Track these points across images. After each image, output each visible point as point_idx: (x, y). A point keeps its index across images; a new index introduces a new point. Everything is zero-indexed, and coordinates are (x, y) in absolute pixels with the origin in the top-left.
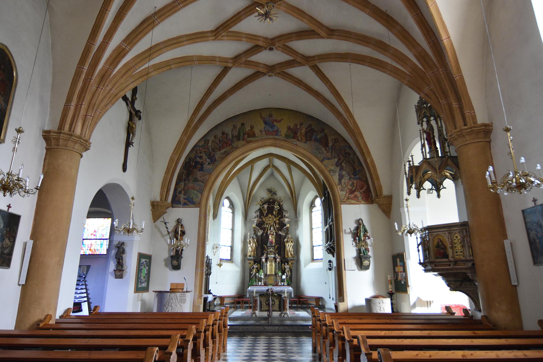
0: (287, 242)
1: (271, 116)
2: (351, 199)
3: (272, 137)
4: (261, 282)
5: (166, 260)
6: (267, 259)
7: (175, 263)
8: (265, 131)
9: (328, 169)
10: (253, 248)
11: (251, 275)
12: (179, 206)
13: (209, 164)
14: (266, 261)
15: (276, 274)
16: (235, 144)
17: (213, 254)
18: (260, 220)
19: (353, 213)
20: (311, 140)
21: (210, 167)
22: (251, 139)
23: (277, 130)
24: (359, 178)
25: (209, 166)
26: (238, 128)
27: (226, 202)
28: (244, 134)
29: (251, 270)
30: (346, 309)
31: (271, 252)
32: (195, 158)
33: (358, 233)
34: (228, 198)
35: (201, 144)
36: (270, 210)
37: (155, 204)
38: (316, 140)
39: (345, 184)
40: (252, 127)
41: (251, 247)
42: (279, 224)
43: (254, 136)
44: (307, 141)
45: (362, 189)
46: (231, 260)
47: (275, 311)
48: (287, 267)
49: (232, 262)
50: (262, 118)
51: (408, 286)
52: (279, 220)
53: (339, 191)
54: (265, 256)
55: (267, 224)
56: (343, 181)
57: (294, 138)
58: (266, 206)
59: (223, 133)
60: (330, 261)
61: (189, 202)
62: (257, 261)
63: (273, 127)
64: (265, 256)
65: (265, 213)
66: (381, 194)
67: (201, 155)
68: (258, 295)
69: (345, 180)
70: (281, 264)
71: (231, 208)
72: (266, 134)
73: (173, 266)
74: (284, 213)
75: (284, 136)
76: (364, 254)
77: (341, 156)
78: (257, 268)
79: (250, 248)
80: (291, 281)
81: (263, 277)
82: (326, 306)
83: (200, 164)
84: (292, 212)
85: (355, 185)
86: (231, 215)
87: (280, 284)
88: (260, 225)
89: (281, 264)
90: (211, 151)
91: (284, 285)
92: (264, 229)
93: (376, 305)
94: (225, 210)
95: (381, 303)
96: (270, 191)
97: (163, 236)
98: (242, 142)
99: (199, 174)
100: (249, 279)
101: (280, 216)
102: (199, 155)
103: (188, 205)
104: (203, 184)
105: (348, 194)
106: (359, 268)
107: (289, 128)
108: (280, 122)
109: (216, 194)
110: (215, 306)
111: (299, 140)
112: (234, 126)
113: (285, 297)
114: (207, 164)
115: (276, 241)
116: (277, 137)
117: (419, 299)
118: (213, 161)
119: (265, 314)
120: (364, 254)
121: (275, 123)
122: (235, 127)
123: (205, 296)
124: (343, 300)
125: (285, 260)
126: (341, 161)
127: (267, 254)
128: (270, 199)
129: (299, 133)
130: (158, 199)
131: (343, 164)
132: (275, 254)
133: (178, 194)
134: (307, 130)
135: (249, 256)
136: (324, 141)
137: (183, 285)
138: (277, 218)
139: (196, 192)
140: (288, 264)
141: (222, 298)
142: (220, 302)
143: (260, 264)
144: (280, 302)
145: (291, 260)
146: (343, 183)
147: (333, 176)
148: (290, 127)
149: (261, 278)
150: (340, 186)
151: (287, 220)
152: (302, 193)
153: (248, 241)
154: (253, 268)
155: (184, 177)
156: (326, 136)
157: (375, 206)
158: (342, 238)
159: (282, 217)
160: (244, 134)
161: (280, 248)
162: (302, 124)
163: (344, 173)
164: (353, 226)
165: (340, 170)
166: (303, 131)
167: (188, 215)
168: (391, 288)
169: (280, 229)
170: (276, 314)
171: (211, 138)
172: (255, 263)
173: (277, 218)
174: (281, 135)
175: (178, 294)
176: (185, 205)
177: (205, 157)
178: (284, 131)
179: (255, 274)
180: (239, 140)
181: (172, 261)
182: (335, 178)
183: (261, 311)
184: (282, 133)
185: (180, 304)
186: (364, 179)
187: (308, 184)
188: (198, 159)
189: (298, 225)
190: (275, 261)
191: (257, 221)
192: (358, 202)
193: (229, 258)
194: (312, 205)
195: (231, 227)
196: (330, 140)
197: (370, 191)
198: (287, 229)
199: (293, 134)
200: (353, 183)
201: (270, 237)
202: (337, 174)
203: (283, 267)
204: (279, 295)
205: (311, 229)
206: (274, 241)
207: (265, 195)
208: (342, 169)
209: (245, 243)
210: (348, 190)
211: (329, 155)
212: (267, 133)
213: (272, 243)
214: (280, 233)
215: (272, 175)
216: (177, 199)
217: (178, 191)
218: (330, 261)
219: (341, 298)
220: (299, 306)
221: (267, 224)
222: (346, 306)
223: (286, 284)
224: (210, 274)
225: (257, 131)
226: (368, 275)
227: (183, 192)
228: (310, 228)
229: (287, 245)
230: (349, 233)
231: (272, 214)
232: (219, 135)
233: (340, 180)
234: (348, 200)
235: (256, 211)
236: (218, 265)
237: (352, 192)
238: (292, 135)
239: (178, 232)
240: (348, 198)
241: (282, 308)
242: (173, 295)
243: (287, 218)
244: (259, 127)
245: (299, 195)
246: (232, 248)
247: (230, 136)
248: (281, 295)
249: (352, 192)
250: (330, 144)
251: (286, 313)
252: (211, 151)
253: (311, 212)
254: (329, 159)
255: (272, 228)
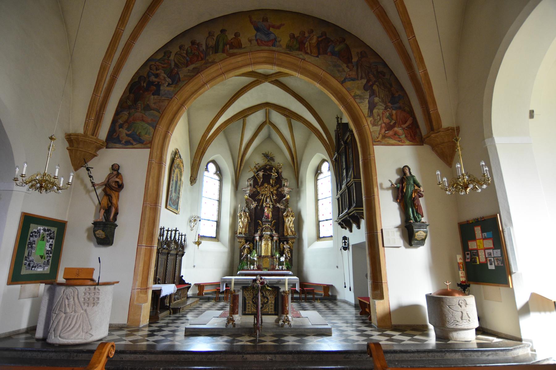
0: (287, 216)
1: (265, 20)
2: (389, 137)
3: (267, 48)
4: (254, 265)
5: (88, 230)
6: (261, 237)
7: (101, 233)
8: (257, 40)
9: (353, 94)
10: (245, 224)
11: (241, 256)
12: (118, 145)
13: (169, 85)
14: (261, 239)
15: (272, 256)
16: (210, 58)
17: (189, 228)
18: (254, 190)
19: (390, 160)
20: (327, 54)
21: (171, 89)
22: (235, 51)
23: (275, 39)
24: (400, 108)
25: (169, 88)
26: (216, 36)
27: (212, 167)
28: (225, 45)
29: (241, 251)
30: (387, 310)
31: (266, 228)
32: (149, 76)
33: (403, 188)
34: (214, 162)
35: (160, 56)
36: (266, 178)
37: (72, 137)
38: (333, 53)
39: (378, 115)
40: (237, 35)
41: (242, 223)
42: (277, 195)
43: (240, 46)
44: (319, 54)
45: (405, 123)
46: (216, 238)
47: (268, 314)
48: (286, 246)
49: (218, 241)
50: (252, 23)
51: (510, 273)
52: (277, 190)
53: (371, 126)
54: (259, 233)
55: (262, 195)
56: (375, 111)
57: (300, 49)
58: (261, 174)
59: (193, 43)
60: (345, 238)
61: (135, 140)
62: (250, 239)
63: (268, 34)
64: (259, 233)
65: (260, 181)
66: (440, 125)
67: (158, 72)
68: (239, 287)
69: (379, 110)
70: (279, 243)
71: (217, 175)
72: (258, 43)
73: (97, 238)
74: (283, 182)
75: (284, 46)
76: (416, 221)
77: (371, 76)
78: (249, 248)
79: (240, 224)
80: (291, 264)
81: (256, 259)
82: (339, 297)
83: (156, 85)
84: (293, 181)
85: (394, 117)
86: (218, 183)
87: (277, 268)
88: (254, 196)
89: (279, 243)
90: (173, 66)
91: (282, 270)
92: (259, 201)
93: (454, 308)
94: (209, 178)
95: (463, 305)
96: (266, 156)
97: (88, 192)
98: (220, 55)
99: (152, 99)
100: (239, 261)
101: (278, 186)
102: (155, 72)
103: (132, 144)
104: (155, 113)
105: (383, 130)
106: (407, 245)
107: (292, 37)
108: (278, 28)
109: (195, 151)
110: (188, 298)
111: (307, 53)
112: (209, 33)
113: (284, 292)
114: (166, 85)
115: (273, 215)
116: (274, 48)
117: (534, 296)
118: (175, 80)
119: (250, 320)
120: (416, 221)
121: (272, 30)
122: (211, 34)
123: (157, 287)
124: (381, 297)
125: (283, 239)
126: (371, 83)
127: (262, 231)
128: (266, 165)
129: (307, 44)
130: (81, 131)
131: (375, 87)
132: (272, 231)
133: (117, 128)
134: (320, 39)
135: (240, 233)
136: (345, 56)
137: (92, 271)
138: (275, 188)
139: (147, 125)
140: (287, 243)
141: (200, 287)
142: (198, 292)
143: (253, 243)
144: (276, 300)
145: (291, 238)
146: (375, 115)
147: (360, 105)
148: (294, 35)
149: (254, 260)
150: (371, 119)
151: (286, 190)
152: (305, 158)
153: (239, 215)
154: (244, 248)
155: (129, 103)
156: (348, 49)
157: (426, 149)
158: (376, 197)
159: (281, 186)
160: (225, 45)
161: (278, 223)
162: (312, 31)
163: (376, 99)
164: (395, 178)
165: (370, 97)
166: (314, 41)
167: (132, 162)
168: (462, 276)
169: (279, 200)
170: (269, 320)
171: (175, 50)
172: (246, 242)
173: (275, 188)
174: (280, 46)
175: (82, 289)
176: (127, 144)
177: (163, 75)
178: (284, 40)
179: (247, 255)
180: (216, 52)
181: (94, 231)
182: (363, 107)
183: (244, 314)
184: (281, 43)
185: (85, 307)
186: (407, 108)
187: (316, 143)
188: (153, 78)
189: (300, 197)
190: (272, 240)
191: (250, 190)
192: (400, 142)
193: (214, 235)
194: (318, 171)
195: (217, 197)
196: (354, 54)
197: (418, 127)
198: (287, 201)
199: (298, 45)
200: (391, 115)
201: (266, 210)
202: (367, 101)
203: (282, 247)
204: (275, 288)
205: (317, 200)
206: (270, 215)
207: (260, 161)
208: (373, 94)
209: (234, 217)
210: (383, 125)
211: (353, 74)
212: (260, 42)
213: (268, 217)
214: (278, 205)
215: (269, 137)
216: (115, 135)
217: (117, 124)
218: (345, 238)
219: (379, 292)
220: (303, 296)
221: (262, 195)
222: (386, 306)
223: (285, 268)
224: (183, 255)
225: (244, 40)
226: (421, 255)
227: (126, 126)
228: (318, 197)
229: (287, 220)
230: (388, 189)
231: (269, 183)
232: (187, 44)
233: (371, 109)
234: (383, 140)
235: (249, 179)
236: (196, 243)
237: (389, 127)
238: (297, 46)
239: (113, 186)
240: (384, 137)
241: (280, 309)
242: (70, 290)
243: (287, 187)
244: (248, 34)
245: (301, 160)
246: (218, 223)
247: (204, 47)
248: (278, 289)
249: (389, 127)
250: (355, 60)
251: (288, 320)
252: (173, 66)
253: (316, 180)
254: (353, 80)
255: (268, 200)
